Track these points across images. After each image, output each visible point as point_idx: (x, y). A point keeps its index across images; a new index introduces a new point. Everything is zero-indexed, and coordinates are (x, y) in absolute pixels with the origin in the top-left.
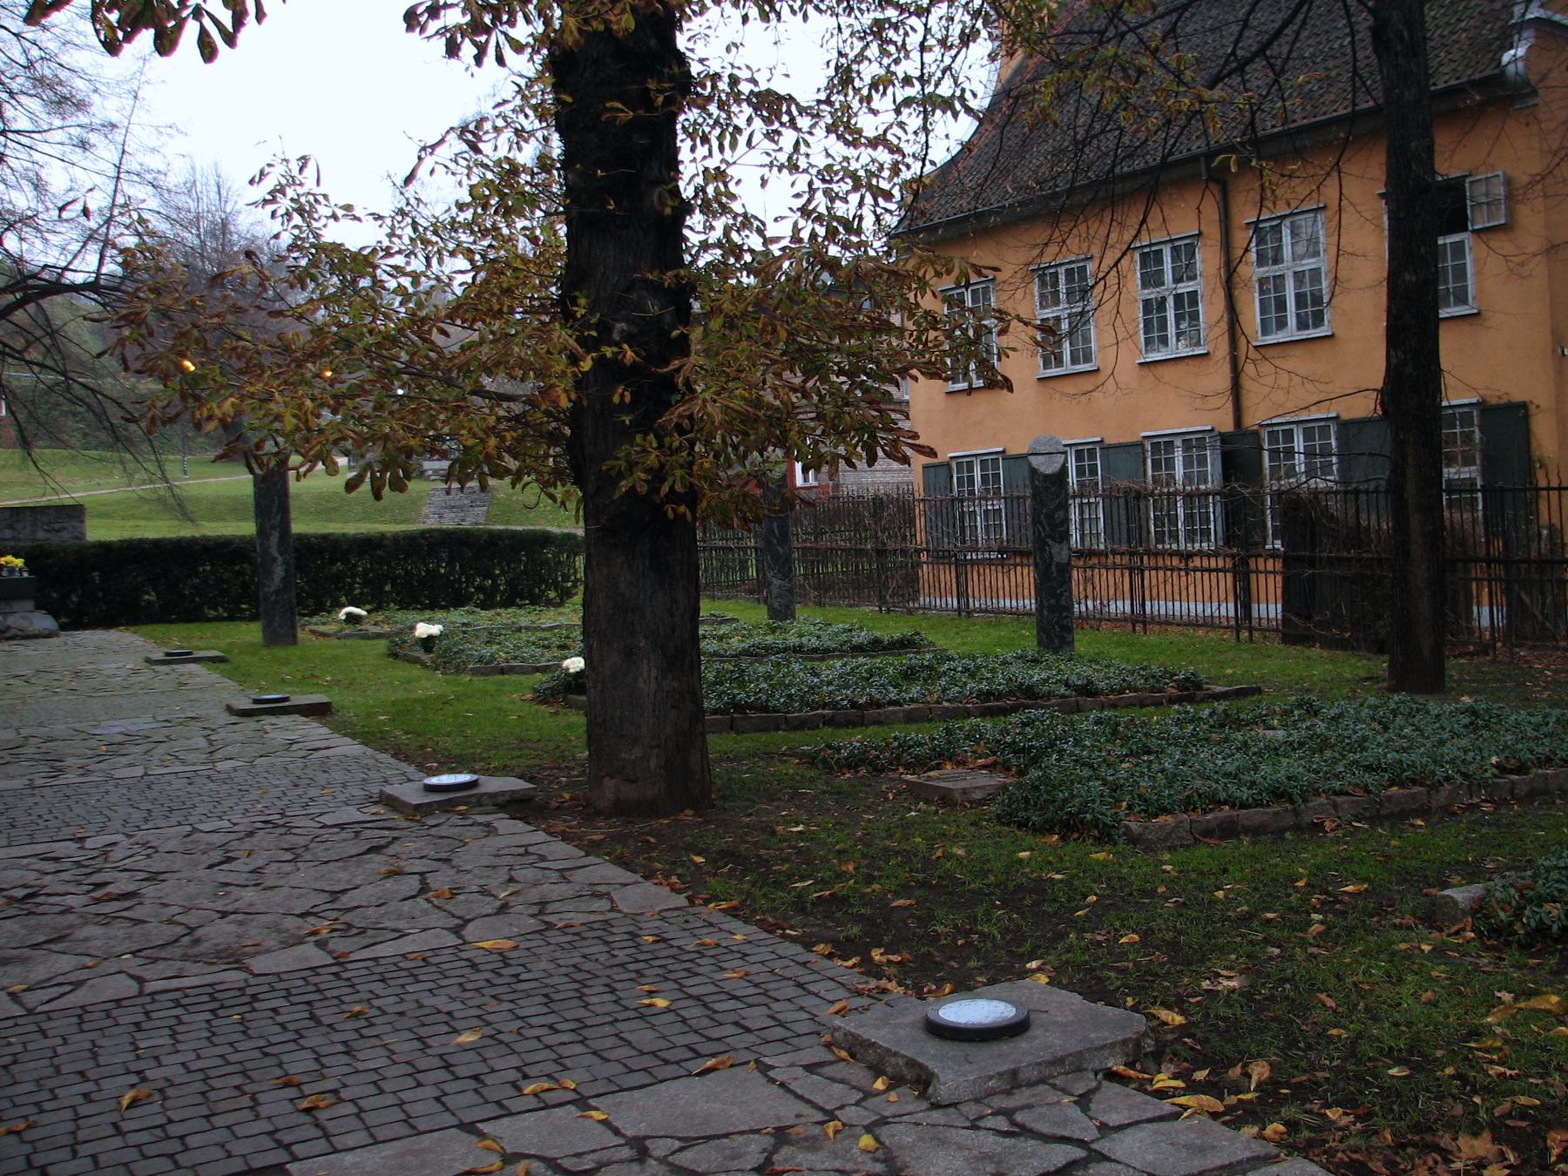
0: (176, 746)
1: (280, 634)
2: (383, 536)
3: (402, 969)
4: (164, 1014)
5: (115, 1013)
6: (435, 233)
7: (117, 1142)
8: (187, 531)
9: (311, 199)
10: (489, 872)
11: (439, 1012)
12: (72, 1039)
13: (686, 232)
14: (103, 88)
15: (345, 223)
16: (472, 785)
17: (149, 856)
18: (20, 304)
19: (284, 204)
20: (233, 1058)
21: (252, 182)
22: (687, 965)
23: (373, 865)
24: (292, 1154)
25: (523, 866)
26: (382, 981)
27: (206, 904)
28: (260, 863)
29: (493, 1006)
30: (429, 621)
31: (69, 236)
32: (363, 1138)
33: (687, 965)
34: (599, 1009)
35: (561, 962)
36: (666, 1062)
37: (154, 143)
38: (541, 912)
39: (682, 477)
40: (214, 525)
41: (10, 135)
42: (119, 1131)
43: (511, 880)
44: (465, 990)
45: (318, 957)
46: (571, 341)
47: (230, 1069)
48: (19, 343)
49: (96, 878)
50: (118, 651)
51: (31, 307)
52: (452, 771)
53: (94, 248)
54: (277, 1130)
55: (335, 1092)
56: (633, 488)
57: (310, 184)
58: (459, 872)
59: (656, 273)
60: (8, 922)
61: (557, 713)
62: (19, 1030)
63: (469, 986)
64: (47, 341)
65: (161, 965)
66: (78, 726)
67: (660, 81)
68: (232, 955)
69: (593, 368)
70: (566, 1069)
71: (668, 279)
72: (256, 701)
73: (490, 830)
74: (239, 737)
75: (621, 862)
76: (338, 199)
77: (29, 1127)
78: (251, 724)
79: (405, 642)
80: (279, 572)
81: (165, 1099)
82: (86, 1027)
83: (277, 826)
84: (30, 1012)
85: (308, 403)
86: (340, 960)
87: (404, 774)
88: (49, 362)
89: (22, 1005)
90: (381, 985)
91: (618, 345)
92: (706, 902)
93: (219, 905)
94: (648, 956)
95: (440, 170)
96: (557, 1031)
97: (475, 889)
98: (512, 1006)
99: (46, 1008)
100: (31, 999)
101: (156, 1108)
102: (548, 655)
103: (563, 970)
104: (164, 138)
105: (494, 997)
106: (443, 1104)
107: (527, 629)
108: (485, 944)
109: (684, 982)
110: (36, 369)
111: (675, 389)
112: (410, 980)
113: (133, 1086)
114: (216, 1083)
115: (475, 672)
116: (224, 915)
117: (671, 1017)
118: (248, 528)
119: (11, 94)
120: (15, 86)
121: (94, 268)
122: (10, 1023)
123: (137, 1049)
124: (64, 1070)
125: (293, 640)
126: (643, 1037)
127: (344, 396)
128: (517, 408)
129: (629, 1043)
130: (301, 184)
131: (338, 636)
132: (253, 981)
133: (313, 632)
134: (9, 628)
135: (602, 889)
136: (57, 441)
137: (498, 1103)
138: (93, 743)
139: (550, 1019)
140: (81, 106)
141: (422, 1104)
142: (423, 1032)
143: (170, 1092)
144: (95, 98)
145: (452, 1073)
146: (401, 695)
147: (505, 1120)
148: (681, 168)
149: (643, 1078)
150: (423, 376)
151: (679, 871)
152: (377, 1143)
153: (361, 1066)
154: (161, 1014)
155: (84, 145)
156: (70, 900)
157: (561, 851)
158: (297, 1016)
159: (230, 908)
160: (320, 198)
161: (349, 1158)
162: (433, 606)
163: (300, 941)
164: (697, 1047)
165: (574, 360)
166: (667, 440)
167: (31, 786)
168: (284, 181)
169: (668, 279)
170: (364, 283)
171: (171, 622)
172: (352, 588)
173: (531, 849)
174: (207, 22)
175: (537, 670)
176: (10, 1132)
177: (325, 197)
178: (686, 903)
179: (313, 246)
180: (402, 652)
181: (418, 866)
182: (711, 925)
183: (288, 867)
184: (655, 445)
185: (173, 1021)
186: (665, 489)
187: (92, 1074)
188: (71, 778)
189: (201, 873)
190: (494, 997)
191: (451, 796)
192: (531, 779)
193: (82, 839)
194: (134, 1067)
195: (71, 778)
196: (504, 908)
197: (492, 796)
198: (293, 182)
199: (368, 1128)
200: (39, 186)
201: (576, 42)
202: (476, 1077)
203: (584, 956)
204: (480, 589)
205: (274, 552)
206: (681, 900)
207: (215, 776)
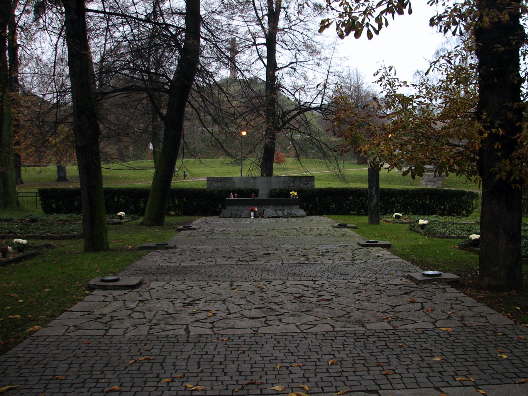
0: (343, 254)
1: (374, 221)
2: (408, 190)
3: (415, 333)
4: (340, 338)
5: (326, 336)
6: (434, 91)
7: (328, 374)
8: (345, 186)
9: (393, 80)
10: (444, 305)
11: (428, 349)
12: (313, 341)
13: (521, 89)
14: (324, 47)
15: (404, 88)
16: (439, 275)
17: (335, 288)
18: (298, 114)
19: (384, 81)
20: (361, 355)
21: (374, 75)
22: (514, 345)
23: (405, 299)
24: (380, 387)
25: (456, 304)
26: (409, 336)
27: (352, 305)
28: (369, 294)
29: (446, 349)
30: (423, 219)
31: (314, 93)
32: (402, 386)
33: (514, 345)
34: (482, 355)
35: (469, 338)
36: (506, 377)
37: (339, 63)
38: (462, 320)
39: (519, 175)
40: (353, 184)
41: (298, 63)
42: (328, 372)
43: (452, 308)
44: (436, 343)
45: (388, 326)
46: (481, 127)
47: (361, 358)
48: (297, 126)
49: (319, 293)
50: (324, 223)
51: (302, 115)
52: (431, 270)
53: (320, 96)
54: (375, 379)
55: (394, 370)
56: (501, 178)
57: (393, 75)
58: (434, 303)
59: (511, 103)
60: (294, 304)
61: (467, 253)
62: (299, 336)
63: (438, 342)
64: (305, 125)
65: (339, 323)
66: (312, 246)
67: (514, 36)
68: (361, 322)
69: (488, 136)
70: (471, 374)
71: (516, 105)
72: (367, 242)
73: (445, 291)
74: (361, 253)
75: (489, 306)
76: (402, 79)
77: (303, 365)
78: (365, 249)
79: (415, 225)
80: (375, 200)
81: (341, 364)
82: (317, 338)
83: (374, 283)
84: (302, 332)
85: (392, 147)
86: (395, 328)
87: (415, 269)
88: (306, 131)
89: (300, 329)
90: (408, 338)
91: (497, 128)
92: (521, 323)
93: (357, 306)
94: (500, 340)
95: (436, 69)
96: (468, 361)
97: (439, 310)
98: (452, 350)
99: (306, 331)
100: (303, 328)
101: (339, 366)
102: (464, 233)
103: (470, 341)
104: (342, 61)
105: (446, 346)
106: (429, 380)
107: (456, 223)
108: (443, 329)
109: (513, 350)
110: (302, 134)
111: (516, 144)
112: (418, 337)
113: (332, 359)
114: (356, 362)
115: (438, 237)
116: (358, 309)
117: (508, 362)
118: (365, 186)
119: (299, 51)
120: (300, 48)
121: (320, 102)
122: (297, 334)
123: (333, 347)
124: (312, 350)
125: (379, 223)
126: (498, 367)
127: (403, 144)
128: (461, 149)
129: (493, 369)
130: (390, 75)
131: (393, 222)
132: (367, 331)
133: (384, 220)
134: (292, 214)
135: (484, 315)
136: (307, 156)
137: (447, 382)
138: (317, 251)
139: (466, 356)
140: (318, 53)
141: (422, 378)
142: (422, 355)
143: (343, 362)
144: (322, 50)
145: (432, 370)
146: (413, 243)
147: (450, 388)
148: (520, 66)
149: (498, 382)
150: (429, 138)
151: (511, 311)
152: (407, 388)
153: (402, 363)
154: (340, 338)
155: (318, 64)
156: (312, 299)
157: (468, 299)
158: (381, 344)
159: (360, 307)
160: (396, 80)
161: (398, 392)
162: (424, 214)
163: (382, 321)
164: (518, 374)
165: (481, 133)
166: (513, 161)
167: (300, 263)
168: (384, 75)
169: (516, 105)
170: (410, 107)
171: (339, 214)
172: (397, 207)
173: (459, 299)
174: (370, 28)
175: (460, 238)
176: (298, 366)
177: (398, 79)
178: (513, 323)
179: (393, 95)
180: (414, 229)
181: (421, 300)
182: (523, 331)
183: (378, 296)
184: (509, 163)
185: (343, 341)
186: (512, 178)
187: (320, 353)
188: (311, 261)
189: (351, 295)
190: (446, 346)
191: (432, 278)
192: (458, 275)
193: (315, 281)
194: (332, 353)
195: (311, 261)
196: (449, 317)
197: (445, 279)
198: (387, 75)
199: (404, 383)
200: (305, 78)
201: (489, 26)
202: (440, 372)
203: (477, 337)
204: (440, 209)
205: (374, 194)
206: (512, 322)
207: (355, 265)
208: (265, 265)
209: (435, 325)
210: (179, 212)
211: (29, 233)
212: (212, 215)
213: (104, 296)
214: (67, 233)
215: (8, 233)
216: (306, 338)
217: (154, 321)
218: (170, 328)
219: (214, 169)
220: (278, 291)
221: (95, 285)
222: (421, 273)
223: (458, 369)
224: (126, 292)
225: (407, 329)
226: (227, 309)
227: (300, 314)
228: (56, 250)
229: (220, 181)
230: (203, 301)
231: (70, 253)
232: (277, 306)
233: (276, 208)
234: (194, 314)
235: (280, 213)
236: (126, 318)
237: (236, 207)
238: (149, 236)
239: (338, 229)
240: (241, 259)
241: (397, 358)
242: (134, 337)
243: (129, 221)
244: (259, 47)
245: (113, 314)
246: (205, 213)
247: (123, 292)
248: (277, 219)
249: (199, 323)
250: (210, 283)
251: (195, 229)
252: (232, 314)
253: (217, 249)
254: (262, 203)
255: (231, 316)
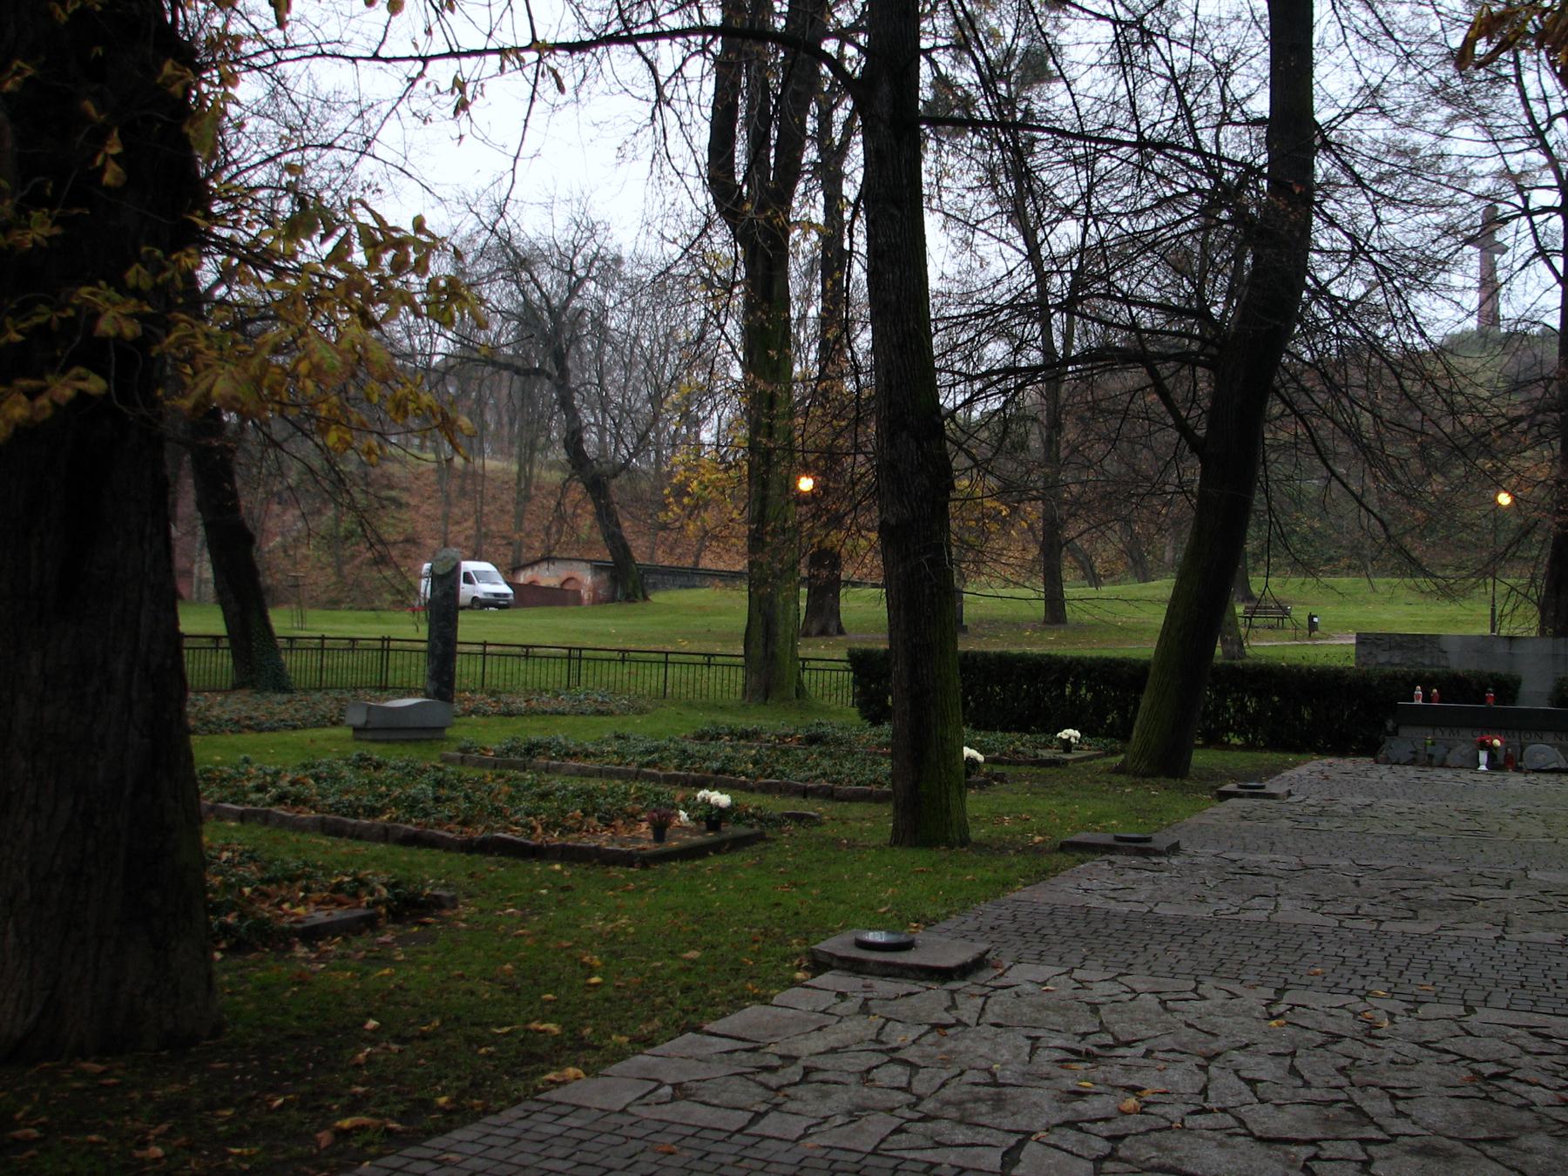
60: (1458, 1103)
156: (1537, 1095)
208: (1432, 940)
210: (1255, 738)
211: (769, 776)
212: (1360, 753)
214: (874, 781)
215: (717, 772)
217: (929, 1106)
218: (960, 1139)
219: (1411, 609)
220: (1424, 1045)
221: (831, 955)
224: (916, 989)
227: (1460, 1147)
228: (817, 830)
229: (1400, 646)
231: (852, 845)
232: (1387, 1105)
234: (1079, 1094)
236: (852, 1079)
237: (1430, 731)
238: (1107, 809)
240: (1366, 908)
242: (823, 1152)
243: (1090, 758)
244: (1537, 219)
246: (1339, 746)
247: (906, 986)
250: (1207, 987)
251: (1272, 796)
252: (1211, 1111)
253: (1306, 867)
254: (1533, 723)
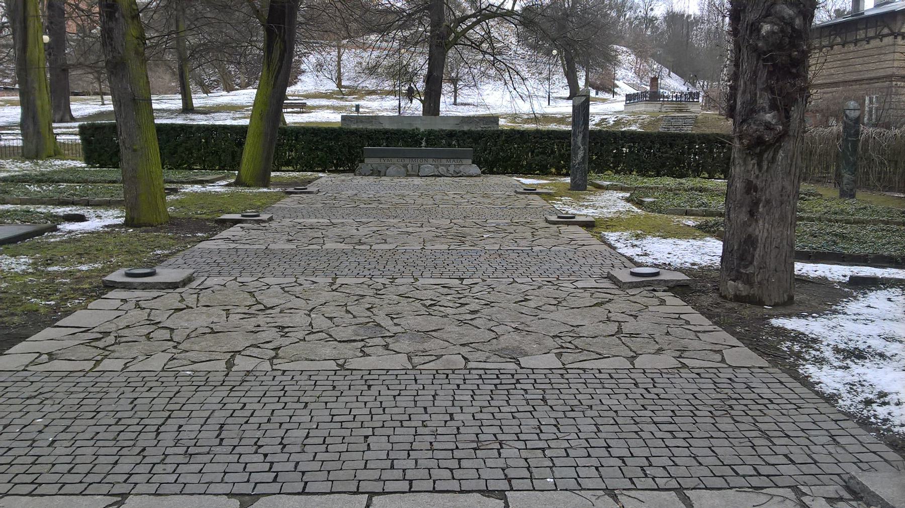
17: (489, 293)
18: (478, 23)
43: (668, 333)
66: (477, 221)
73: (663, 302)
80: (581, 154)
97: (647, 336)
122: (404, 372)
132: (519, 371)
173: (682, 316)
209: (633, 365)
213: (122, 300)
216: (416, 380)
222: (630, 270)
223: (655, 452)
224: (161, 294)
225: (584, 370)
226: (311, 324)
230: (278, 310)
233: (438, 162)
235: (442, 170)
239: (522, 196)
241: (555, 425)
245: (121, 333)
247: (155, 293)
248: (438, 179)
249: (255, 350)
255: (312, 336)
